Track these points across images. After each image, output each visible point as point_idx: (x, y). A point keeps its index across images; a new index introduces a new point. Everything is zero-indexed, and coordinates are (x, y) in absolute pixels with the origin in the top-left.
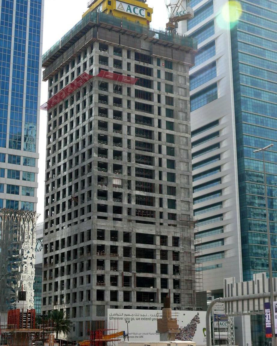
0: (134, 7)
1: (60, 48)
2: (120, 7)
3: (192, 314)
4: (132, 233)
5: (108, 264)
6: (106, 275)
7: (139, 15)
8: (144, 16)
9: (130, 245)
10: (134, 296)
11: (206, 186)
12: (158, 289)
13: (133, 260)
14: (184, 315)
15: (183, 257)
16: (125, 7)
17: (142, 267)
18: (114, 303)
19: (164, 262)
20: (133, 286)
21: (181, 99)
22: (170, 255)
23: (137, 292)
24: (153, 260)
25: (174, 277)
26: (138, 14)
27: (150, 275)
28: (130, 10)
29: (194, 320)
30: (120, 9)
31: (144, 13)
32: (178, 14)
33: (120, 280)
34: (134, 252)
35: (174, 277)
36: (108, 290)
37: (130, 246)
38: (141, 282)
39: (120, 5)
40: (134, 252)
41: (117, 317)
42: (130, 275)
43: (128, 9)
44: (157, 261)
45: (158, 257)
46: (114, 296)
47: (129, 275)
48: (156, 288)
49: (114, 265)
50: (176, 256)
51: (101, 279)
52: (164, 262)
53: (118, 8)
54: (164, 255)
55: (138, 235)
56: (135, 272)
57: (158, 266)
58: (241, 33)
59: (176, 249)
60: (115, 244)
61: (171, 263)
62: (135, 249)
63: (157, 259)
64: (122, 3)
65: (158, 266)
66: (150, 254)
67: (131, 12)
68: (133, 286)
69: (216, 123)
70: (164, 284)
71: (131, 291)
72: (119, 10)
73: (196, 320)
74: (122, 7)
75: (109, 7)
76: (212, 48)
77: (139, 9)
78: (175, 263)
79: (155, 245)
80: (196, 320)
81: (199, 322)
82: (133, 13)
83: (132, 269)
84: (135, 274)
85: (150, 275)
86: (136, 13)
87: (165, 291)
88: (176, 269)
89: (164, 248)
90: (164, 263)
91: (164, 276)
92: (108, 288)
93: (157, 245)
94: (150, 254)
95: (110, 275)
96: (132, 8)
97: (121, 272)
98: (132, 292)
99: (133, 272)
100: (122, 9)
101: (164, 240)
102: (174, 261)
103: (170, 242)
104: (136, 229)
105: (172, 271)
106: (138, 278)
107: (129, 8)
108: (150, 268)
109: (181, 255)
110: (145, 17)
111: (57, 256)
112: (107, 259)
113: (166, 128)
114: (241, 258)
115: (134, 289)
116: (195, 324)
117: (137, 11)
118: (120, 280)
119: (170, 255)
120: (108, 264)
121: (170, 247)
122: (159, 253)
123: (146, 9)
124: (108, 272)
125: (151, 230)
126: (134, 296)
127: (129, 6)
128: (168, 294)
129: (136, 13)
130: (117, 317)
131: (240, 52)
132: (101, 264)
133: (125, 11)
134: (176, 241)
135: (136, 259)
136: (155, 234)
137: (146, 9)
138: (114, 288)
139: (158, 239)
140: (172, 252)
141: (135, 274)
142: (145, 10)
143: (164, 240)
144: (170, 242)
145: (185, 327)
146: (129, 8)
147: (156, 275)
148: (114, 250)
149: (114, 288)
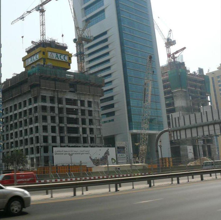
0: (60, 55)
1: (10, 86)
2: (51, 56)
3: (104, 150)
4: (63, 98)
5: (49, 119)
6: (48, 126)
7: (64, 60)
8: (67, 60)
9: (62, 106)
10: (66, 139)
11: (104, 71)
12: (81, 135)
13: (65, 116)
14: (100, 150)
15: (94, 114)
16: (54, 55)
17: (70, 121)
18: (54, 144)
19: (83, 117)
20: (65, 133)
21: (97, 119)
22: (87, 113)
23: (68, 137)
24: (77, 116)
25: (90, 127)
26: (63, 60)
27: (75, 126)
28: (58, 57)
29: (106, 153)
30: (51, 57)
31: (67, 58)
32: (87, 37)
33: (57, 128)
34: (65, 111)
35: (90, 127)
36: (50, 136)
37: (62, 107)
38: (71, 130)
39: (51, 54)
40: (65, 111)
41: (59, 153)
42: (63, 126)
43: (56, 57)
44: (80, 116)
45: (80, 114)
46: (54, 139)
47: (62, 126)
48: (79, 134)
49: (53, 119)
50: (90, 113)
51: (45, 128)
52: (83, 117)
53: (50, 57)
54: (83, 112)
55: (67, 99)
56: (66, 124)
57: (80, 120)
58: (127, 48)
59: (91, 109)
60: (53, 105)
61: (87, 118)
62: (66, 108)
63: (79, 115)
64: (52, 53)
65: (80, 120)
66: (75, 112)
67: (58, 58)
68: (65, 133)
69: (105, 33)
70: (84, 131)
71: (64, 136)
72: (50, 58)
73: (107, 153)
74: (53, 56)
75: (44, 56)
76: (102, 14)
77: (63, 56)
78: (90, 118)
79: (78, 106)
80: (107, 153)
81: (109, 155)
82: (60, 59)
83: (65, 121)
84: (66, 125)
85: (75, 126)
86: (62, 59)
87: (85, 136)
88: (91, 121)
89: (83, 108)
90: (83, 118)
91: (84, 126)
92: (50, 134)
93: (78, 106)
94: (75, 112)
95: (51, 126)
96: (59, 55)
97: (58, 124)
98: (65, 137)
99: (65, 123)
100: (52, 57)
101: (82, 103)
102: (89, 117)
103: (86, 104)
104: (65, 96)
105: (89, 123)
106: (68, 128)
107: (57, 56)
108: (75, 121)
109: (93, 113)
110: (67, 61)
111: (17, 142)
112: (48, 115)
113: (86, 110)
114: (124, 84)
115: (66, 134)
116: (107, 156)
117: (62, 57)
118: (57, 128)
119: (87, 113)
120: (49, 119)
121: (86, 107)
122: (80, 112)
123: (68, 55)
124: (49, 124)
125: (75, 96)
126: (66, 139)
127: (57, 54)
128: (87, 138)
129: (62, 59)
130: (59, 153)
131: (126, 47)
132: (45, 118)
133: (55, 59)
134: (90, 104)
135: (66, 115)
136: (77, 99)
137: (68, 55)
138: (54, 134)
139: (79, 102)
140: (88, 111)
141: (66, 125)
142: (67, 56)
143: (82, 103)
144: (86, 104)
145: (101, 158)
146: (57, 56)
147: (79, 126)
148: (52, 109)
149: (54, 134)
